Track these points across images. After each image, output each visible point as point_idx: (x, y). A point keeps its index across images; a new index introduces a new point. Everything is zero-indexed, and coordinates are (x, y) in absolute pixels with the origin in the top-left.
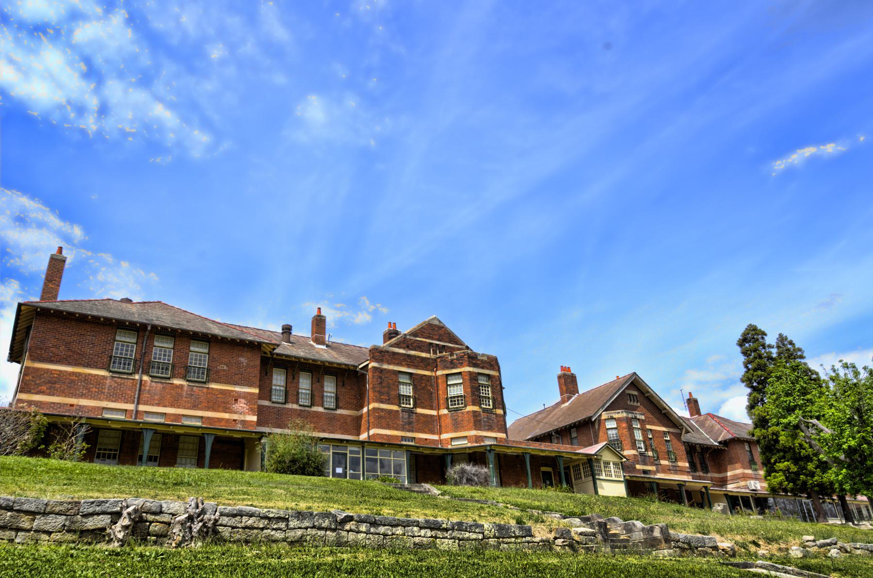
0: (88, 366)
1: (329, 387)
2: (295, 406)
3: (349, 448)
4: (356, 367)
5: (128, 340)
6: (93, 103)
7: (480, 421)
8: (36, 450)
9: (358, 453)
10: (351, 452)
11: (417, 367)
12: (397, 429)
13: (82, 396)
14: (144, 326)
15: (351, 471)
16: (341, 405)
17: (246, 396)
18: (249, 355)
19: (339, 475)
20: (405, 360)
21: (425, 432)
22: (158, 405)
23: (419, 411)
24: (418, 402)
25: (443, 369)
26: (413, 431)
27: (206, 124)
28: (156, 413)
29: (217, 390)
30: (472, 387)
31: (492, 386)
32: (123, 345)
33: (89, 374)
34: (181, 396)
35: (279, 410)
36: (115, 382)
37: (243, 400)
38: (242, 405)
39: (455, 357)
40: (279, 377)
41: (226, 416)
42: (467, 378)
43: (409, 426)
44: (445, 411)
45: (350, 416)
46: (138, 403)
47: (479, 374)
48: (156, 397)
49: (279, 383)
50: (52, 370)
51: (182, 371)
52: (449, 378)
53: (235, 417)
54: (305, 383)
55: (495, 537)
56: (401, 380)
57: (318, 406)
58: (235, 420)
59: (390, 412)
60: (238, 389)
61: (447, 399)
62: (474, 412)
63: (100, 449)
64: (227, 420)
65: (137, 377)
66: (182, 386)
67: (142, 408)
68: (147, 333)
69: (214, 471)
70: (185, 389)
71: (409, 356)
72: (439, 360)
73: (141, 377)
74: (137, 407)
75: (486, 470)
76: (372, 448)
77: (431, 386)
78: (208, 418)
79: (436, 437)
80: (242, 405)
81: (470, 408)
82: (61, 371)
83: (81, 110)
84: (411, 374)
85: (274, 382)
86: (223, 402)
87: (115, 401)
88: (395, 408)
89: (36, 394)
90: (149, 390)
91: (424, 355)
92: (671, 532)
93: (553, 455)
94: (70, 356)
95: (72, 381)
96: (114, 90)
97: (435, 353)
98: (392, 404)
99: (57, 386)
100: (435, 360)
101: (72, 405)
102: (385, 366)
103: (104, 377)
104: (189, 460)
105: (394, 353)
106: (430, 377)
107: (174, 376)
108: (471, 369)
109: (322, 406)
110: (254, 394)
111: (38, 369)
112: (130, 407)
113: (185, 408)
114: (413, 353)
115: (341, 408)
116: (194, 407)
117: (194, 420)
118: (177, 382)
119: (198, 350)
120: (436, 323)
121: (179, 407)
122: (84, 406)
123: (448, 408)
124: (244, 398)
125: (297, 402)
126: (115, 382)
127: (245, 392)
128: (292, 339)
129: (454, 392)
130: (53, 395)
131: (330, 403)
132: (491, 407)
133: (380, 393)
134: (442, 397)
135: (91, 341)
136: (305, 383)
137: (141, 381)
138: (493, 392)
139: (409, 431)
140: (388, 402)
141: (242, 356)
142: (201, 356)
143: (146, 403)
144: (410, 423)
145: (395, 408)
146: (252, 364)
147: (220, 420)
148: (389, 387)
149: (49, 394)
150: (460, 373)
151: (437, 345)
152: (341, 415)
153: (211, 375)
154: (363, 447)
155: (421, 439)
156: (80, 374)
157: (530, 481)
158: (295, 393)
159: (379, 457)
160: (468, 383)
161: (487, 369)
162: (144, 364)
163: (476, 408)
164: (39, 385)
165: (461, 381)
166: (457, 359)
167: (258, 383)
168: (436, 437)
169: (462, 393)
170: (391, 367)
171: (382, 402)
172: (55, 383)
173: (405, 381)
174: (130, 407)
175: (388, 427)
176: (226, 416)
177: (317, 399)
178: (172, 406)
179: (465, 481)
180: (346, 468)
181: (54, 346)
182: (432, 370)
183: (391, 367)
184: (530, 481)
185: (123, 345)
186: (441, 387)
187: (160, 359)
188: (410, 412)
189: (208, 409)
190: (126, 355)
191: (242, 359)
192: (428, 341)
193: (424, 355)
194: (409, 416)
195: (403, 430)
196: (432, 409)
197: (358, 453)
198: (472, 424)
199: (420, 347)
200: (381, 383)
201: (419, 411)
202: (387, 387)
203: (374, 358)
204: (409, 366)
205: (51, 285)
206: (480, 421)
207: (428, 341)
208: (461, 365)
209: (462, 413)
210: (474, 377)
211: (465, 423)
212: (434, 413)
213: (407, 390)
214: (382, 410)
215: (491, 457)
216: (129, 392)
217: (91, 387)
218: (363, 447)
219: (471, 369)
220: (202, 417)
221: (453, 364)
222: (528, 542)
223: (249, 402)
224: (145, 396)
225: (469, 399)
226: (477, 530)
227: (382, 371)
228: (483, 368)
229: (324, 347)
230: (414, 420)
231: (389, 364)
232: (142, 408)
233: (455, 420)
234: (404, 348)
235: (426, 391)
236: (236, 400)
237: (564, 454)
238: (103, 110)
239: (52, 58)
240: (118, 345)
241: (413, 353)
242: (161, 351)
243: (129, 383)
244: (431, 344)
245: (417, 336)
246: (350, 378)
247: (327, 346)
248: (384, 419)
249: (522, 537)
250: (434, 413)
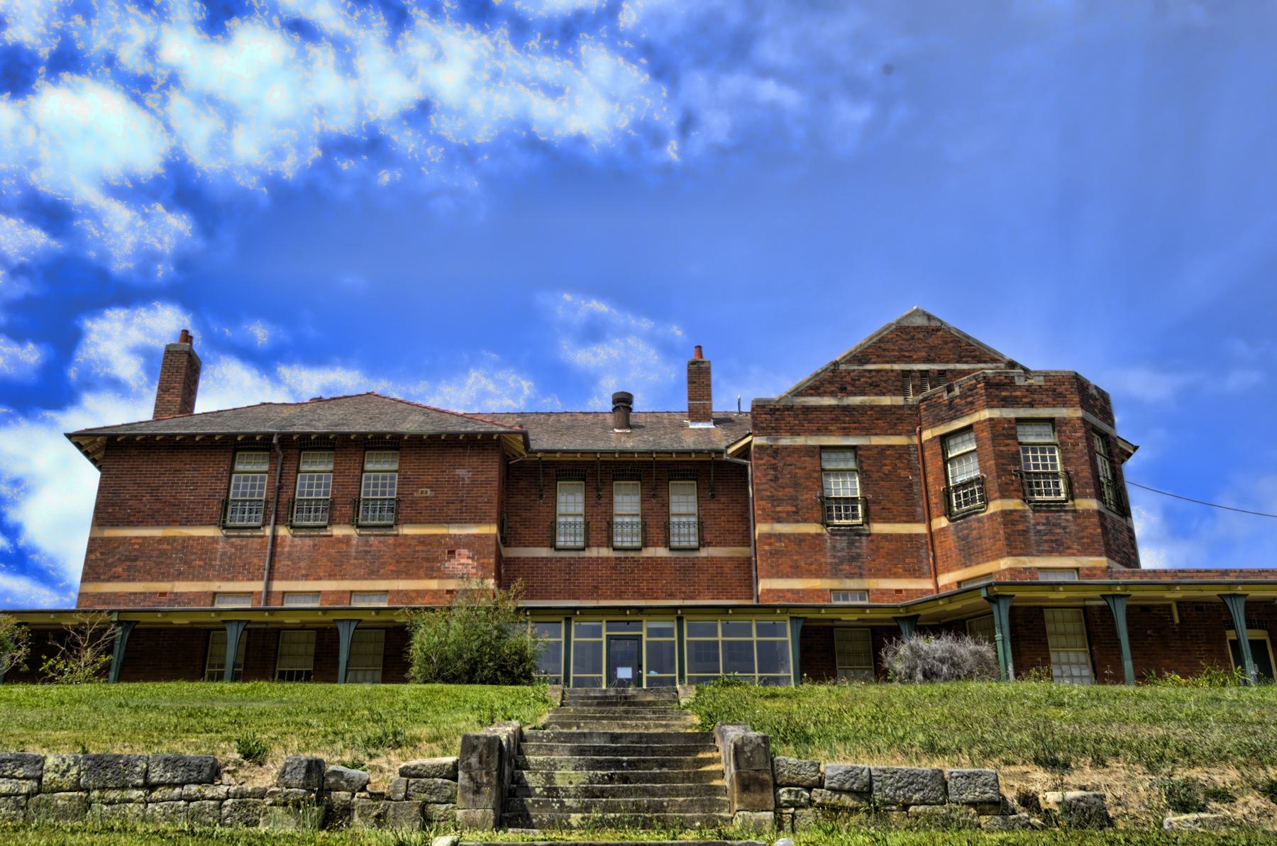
0: (188, 522)
1: (683, 504)
2: (605, 552)
3: (645, 626)
4: (720, 452)
5: (255, 468)
6: (667, 118)
7: (1025, 532)
8: (28, 673)
9: (668, 632)
10: (651, 632)
11: (868, 432)
12: (818, 575)
13: (180, 576)
14: (286, 439)
15: (653, 674)
16: (708, 538)
17: (469, 542)
18: (475, 461)
19: (624, 683)
20: (836, 420)
21: (896, 576)
22: (306, 577)
23: (878, 528)
24: (873, 508)
25: (933, 425)
26: (861, 576)
27: (856, 89)
28: (305, 592)
29: (413, 537)
30: (999, 456)
31: (1062, 445)
32: (246, 479)
33: (190, 538)
34: (348, 556)
35: (570, 562)
36: (233, 545)
37: (465, 552)
38: (463, 561)
39: (957, 391)
40: (571, 499)
41: (433, 585)
42: (986, 435)
43: (853, 564)
44: (941, 522)
45: (731, 559)
46: (270, 579)
47: (1019, 421)
48: (302, 564)
49: (571, 510)
50: (131, 538)
51: (348, 510)
52: (952, 442)
53: (451, 585)
54: (627, 504)
55: (76, 787)
56: (827, 466)
57: (655, 545)
58: (449, 592)
59: (800, 539)
60: (454, 530)
61: (947, 494)
62: (1005, 514)
63: (212, 666)
64: (435, 593)
65: (268, 531)
66: (346, 540)
67: (278, 586)
68: (278, 449)
69: (389, 686)
70: (354, 542)
71: (847, 409)
72: (923, 406)
73: (274, 531)
74: (268, 586)
75: (985, 648)
76: (768, 620)
77: (910, 467)
78: (399, 592)
79: (927, 584)
80: (463, 561)
81: (995, 506)
82: (144, 538)
83: (656, 137)
84: (854, 448)
85: (561, 509)
86: (427, 559)
87: (232, 580)
88: (813, 529)
89: (108, 580)
90: (290, 553)
91: (886, 401)
92: (787, 757)
93: (1211, 593)
94: (159, 511)
95: (163, 553)
96: (696, 84)
97: (918, 390)
98: (805, 521)
99: (140, 563)
100: (915, 408)
101: (163, 594)
102: (785, 441)
103: (214, 540)
104: (369, 674)
105: (808, 409)
106: (908, 447)
107: (332, 522)
108: (996, 413)
109: (667, 544)
110: (487, 536)
111: (110, 540)
112: (258, 586)
113: (354, 578)
114: (856, 400)
115: (709, 544)
116: (372, 574)
117: (375, 598)
118: (338, 531)
119: (381, 467)
120: (920, 321)
121: (343, 578)
122: (182, 594)
123: (948, 513)
124: (466, 546)
125: (609, 543)
126: (233, 545)
127: (468, 536)
128: (633, 421)
129: (965, 472)
130: (134, 580)
131: (685, 535)
132: (1063, 496)
133: (774, 500)
134: (936, 488)
135: (194, 478)
136: (570, 504)
137: (274, 537)
138: (1065, 461)
139: (850, 576)
140: (795, 517)
141: (461, 466)
142: (384, 478)
143: (285, 577)
144: (853, 558)
145: (813, 529)
146: (483, 478)
147: (420, 593)
148: (796, 485)
149: (128, 580)
150: (969, 428)
151: (924, 374)
152: (710, 559)
153: (402, 510)
154: (680, 619)
155: (883, 592)
156: (174, 539)
157: (1128, 665)
158: (604, 525)
159: (720, 638)
160: (988, 447)
161: (1046, 405)
162: (281, 507)
163: (1014, 504)
164: (112, 565)
165: (973, 447)
166: (962, 396)
167: (494, 513)
168: (927, 584)
169: (976, 474)
170: (800, 441)
171: (779, 520)
172: (135, 559)
173: (842, 466)
174: (258, 586)
175: (797, 572)
176: (433, 585)
177: (654, 532)
178: (331, 576)
179: (920, 676)
180: (640, 667)
181: (134, 497)
182: (910, 433)
183: (800, 441)
184: (1128, 665)
185: (246, 479)
186: (933, 465)
187: (310, 493)
188: (854, 532)
189: (397, 575)
190: (252, 494)
191: (461, 472)
192: (897, 367)
193: (886, 401)
194: (851, 544)
195: (835, 573)
196: (912, 519)
197: (668, 632)
198: (1001, 543)
199: (876, 384)
200: (776, 479)
201: (878, 528)
202: (801, 488)
203: (758, 429)
204: (846, 432)
205: (167, 398)
206: (1025, 532)
207: (897, 367)
208: (972, 407)
209: (980, 520)
210: (1003, 432)
211: (987, 542)
212: (920, 529)
213: (847, 487)
214: (780, 537)
215: (1001, 615)
216: (255, 560)
217: (190, 560)
218: (680, 619)
219: (996, 413)
220: (387, 592)
221: (954, 411)
222: (190, 799)
223: (478, 553)
224: (282, 564)
225: (993, 486)
226: (20, 772)
227: (776, 452)
228: (1031, 405)
229: (710, 426)
230: (864, 551)
231: (794, 433)
232: (278, 586)
233: (965, 538)
234: (833, 394)
235: (895, 485)
236: (452, 553)
237: (1240, 590)
238: (688, 124)
239: (600, 62)
240: (238, 479)
241: (856, 400)
242: (311, 478)
243: (255, 543)
244: (906, 374)
245: (868, 362)
246: (717, 476)
247: (717, 422)
248: (798, 556)
249: (172, 785)
250: (920, 529)
